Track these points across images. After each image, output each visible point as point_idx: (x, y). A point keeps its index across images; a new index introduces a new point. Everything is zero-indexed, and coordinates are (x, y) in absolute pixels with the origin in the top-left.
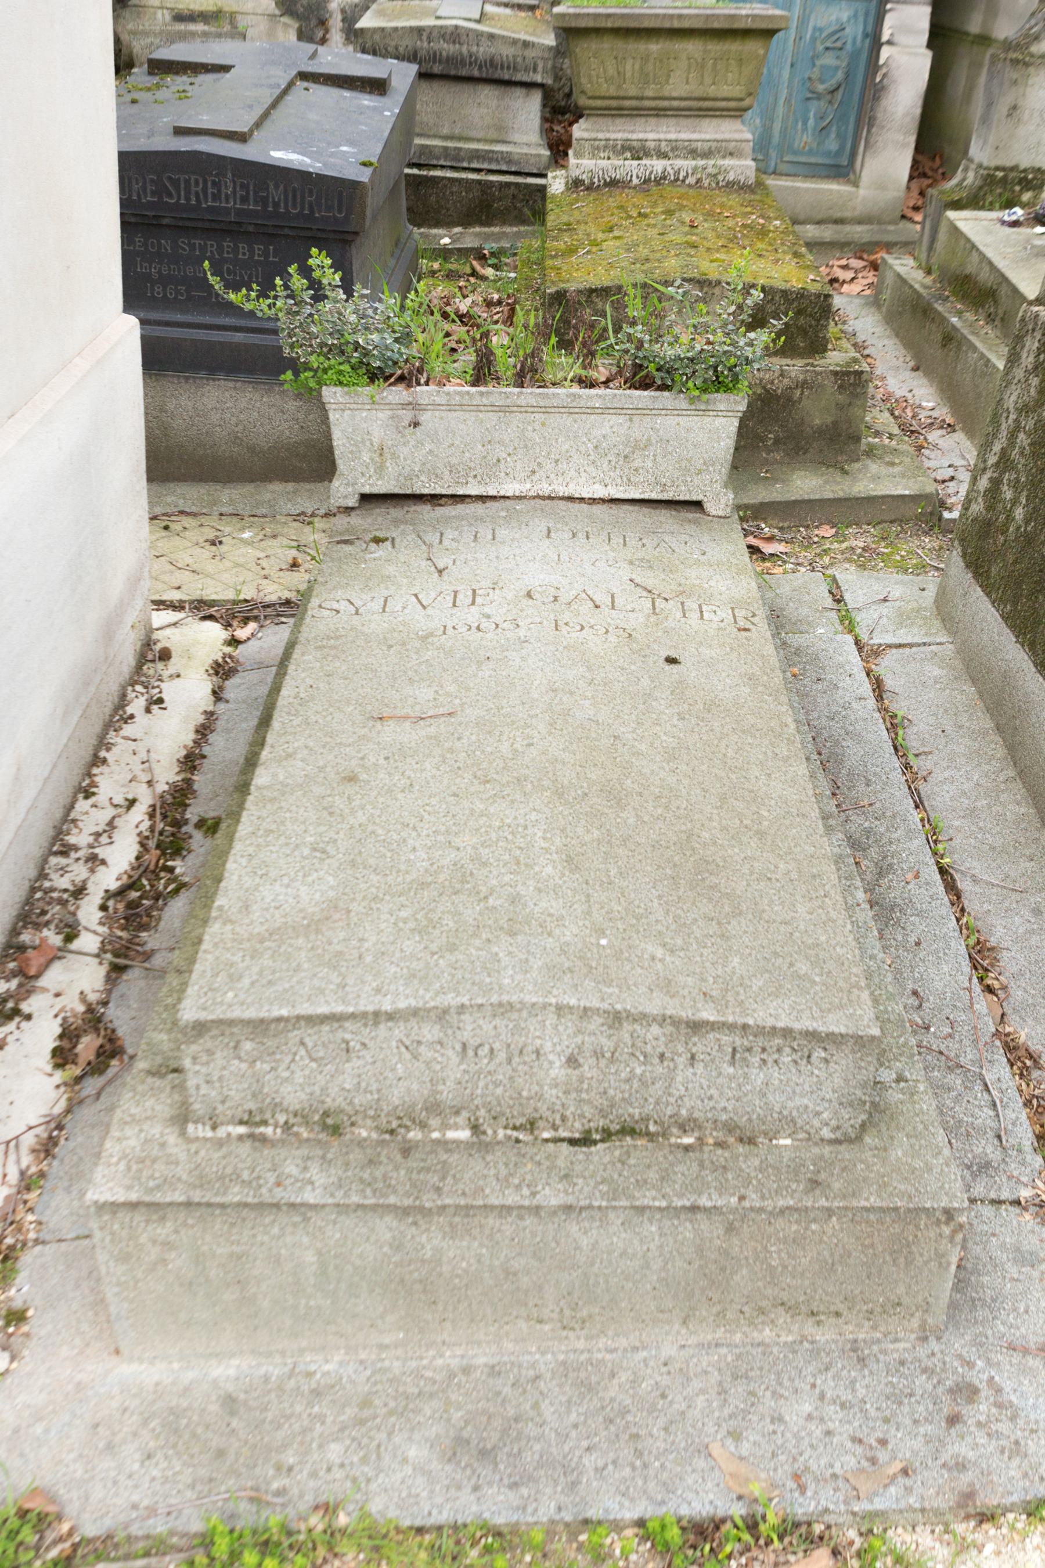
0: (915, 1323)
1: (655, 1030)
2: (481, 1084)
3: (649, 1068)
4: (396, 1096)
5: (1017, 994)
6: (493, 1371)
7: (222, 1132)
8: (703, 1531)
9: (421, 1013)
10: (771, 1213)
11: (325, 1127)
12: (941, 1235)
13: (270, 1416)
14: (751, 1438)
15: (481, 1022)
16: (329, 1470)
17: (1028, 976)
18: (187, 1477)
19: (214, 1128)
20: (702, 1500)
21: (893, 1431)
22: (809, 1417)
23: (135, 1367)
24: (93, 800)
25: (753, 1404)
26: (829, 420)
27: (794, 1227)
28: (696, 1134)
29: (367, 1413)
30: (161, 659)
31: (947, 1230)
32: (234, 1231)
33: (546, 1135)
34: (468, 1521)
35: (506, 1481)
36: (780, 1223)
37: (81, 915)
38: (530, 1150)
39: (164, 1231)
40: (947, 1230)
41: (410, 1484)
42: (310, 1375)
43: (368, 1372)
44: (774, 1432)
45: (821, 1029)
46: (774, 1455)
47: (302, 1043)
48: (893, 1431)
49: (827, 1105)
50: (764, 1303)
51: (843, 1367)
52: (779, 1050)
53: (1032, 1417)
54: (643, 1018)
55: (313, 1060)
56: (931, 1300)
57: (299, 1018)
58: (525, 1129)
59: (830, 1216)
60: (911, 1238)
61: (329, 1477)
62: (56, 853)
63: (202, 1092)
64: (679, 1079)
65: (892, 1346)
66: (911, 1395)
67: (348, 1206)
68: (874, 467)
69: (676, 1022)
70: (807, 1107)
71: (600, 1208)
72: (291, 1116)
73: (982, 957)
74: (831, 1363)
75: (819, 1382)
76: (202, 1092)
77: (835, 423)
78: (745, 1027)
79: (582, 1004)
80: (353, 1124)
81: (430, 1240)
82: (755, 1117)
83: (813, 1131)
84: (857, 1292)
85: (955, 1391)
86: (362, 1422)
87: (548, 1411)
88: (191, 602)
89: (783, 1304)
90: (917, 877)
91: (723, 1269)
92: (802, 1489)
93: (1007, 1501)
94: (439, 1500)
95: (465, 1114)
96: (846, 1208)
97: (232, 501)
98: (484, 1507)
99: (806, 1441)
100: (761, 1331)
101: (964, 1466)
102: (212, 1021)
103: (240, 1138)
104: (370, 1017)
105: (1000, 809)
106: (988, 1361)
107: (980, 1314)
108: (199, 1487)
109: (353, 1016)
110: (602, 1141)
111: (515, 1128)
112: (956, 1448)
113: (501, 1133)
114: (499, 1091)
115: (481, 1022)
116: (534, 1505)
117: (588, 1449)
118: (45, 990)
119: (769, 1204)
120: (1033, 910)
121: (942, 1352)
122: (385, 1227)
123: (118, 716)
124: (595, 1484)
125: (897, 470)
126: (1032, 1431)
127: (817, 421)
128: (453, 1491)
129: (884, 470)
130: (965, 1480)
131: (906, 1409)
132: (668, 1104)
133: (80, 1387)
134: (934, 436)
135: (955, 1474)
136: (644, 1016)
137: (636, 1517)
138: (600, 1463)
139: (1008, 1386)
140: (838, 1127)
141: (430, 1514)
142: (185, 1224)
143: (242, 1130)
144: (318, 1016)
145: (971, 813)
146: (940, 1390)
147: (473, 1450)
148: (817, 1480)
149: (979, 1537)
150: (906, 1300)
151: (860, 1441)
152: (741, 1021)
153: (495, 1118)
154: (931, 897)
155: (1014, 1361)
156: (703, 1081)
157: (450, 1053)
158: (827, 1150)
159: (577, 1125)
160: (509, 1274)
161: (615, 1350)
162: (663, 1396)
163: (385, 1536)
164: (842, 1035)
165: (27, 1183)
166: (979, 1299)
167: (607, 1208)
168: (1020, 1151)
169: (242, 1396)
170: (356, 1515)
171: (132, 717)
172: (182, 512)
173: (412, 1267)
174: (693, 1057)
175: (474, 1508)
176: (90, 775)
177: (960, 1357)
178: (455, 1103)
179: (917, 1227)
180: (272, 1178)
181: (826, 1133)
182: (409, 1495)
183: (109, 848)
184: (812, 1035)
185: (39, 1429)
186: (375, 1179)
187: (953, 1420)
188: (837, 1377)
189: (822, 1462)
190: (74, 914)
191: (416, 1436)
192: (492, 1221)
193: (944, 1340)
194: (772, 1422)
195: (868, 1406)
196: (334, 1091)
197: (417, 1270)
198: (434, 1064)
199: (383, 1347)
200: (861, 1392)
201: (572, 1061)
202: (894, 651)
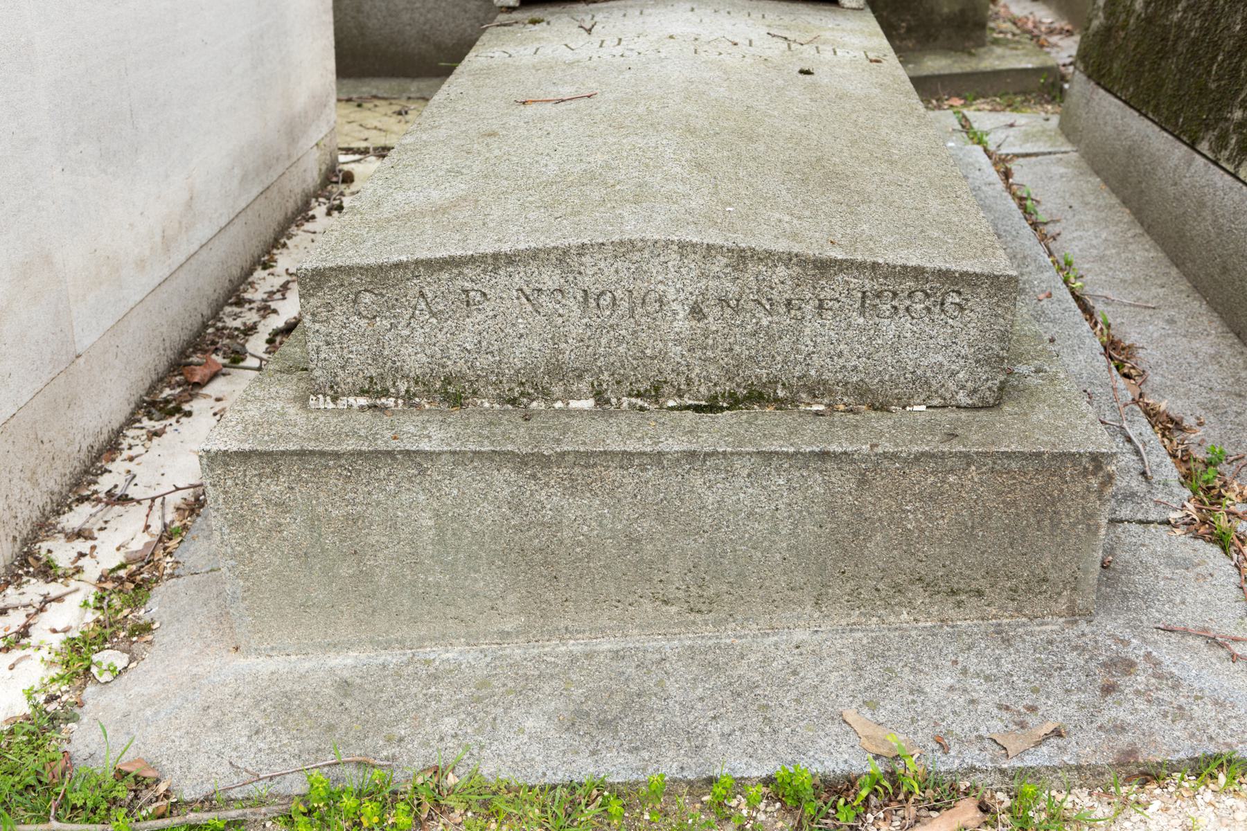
0: (1063, 605)
1: (782, 271)
2: (604, 341)
3: (776, 318)
4: (517, 357)
5: (1154, 379)
6: (617, 655)
7: (342, 403)
8: (837, 788)
9: (541, 255)
10: (905, 460)
11: (446, 397)
12: (1088, 488)
13: (385, 696)
14: (889, 707)
15: (602, 264)
16: (442, 739)
17: (1165, 366)
18: (295, 747)
19: (334, 399)
20: (835, 758)
21: (1043, 699)
22: (951, 688)
23: (252, 659)
24: (271, 270)
25: (890, 679)
26: (957, 8)
27: (931, 479)
28: (826, 401)
29: (484, 692)
30: (344, 182)
31: (1094, 483)
32: (350, 487)
33: (671, 403)
34: (585, 781)
35: (626, 746)
36: (915, 473)
37: (248, 346)
38: (655, 416)
39: (276, 488)
40: (1094, 483)
41: (528, 749)
42: (428, 662)
43: (488, 659)
44: (914, 702)
45: (954, 268)
46: (913, 721)
47: (422, 295)
48: (1043, 699)
49: (962, 362)
50: (900, 579)
51: (987, 647)
52: (910, 296)
53: (1196, 685)
54: (769, 257)
55: (433, 315)
56: (1080, 574)
57: (417, 263)
58: (650, 397)
59: (969, 465)
60: (1056, 493)
61: (442, 745)
62: (231, 304)
63: (323, 356)
64: (807, 331)
65: (1038, 629)
66: (1061, 669)
67: (465, 453)
68: (999, 51)
69: (802, 261)
70: (941, 365)
71: (724, 453)
72: (412, 383)
73: (1116, 351)
74: (973, 644)
75: (960, 659)
76: (323, 356)
77: (962, 12)
78: (875, 266)
79: (705, 242)
80: (475, 393)
81: (550, 497)
82: (887, 378)
83: (948, 396)
84: (999, 564)
85: (1109, 665)
86: (479, 700)
87: (672, 687)
88: (375, 149)
89: (920, 579)
90: (1050, 296)
91: (856, 534)
92: (945, 749)
93: (1175, 758)
94: (555, 763)
95: (588, 378)
96: (985, 454)
97: (419, 90)
98: (602, 769)
99: (949, 709)
100: (898, 614)
101: (1123, 729)
102: (331, 269)
103: (362, 408)
104: (490, 261)
105: (1130, 255)
106: (1144, 640)
107: (1133, 603)
108: (305, 756)
109: (472, 260)
110: (728, 409)
111: (639, 395)
112: (1113, 713)
113: (625, 401)
114: (622, 349)
115: (602, 264)
116: (656, 766)
117: (714, 718)
118: (206, 396)
119: (904, 450)
120: (1167, 321)
121: (1093, 633)
122: (503, 480)
123: (302, 214)
124: (720, 747)
125: (1019, 52)
126: (1197, 698)
127: (946, 10)
128: (569, 756)
129: (1008, 52)
130: (1124, 741)
131: (1056, 681)
132: (796, 362)
133: (195, 677)
134: (1054, 39)
135: (1115, 736)
136: (770, 254)
137: (764, 775)
138: (727, 730)
139: (1167, 660)
140: (975, 391)
141: (544, 774)
142: (299, 479)
143: (363, 401)
144: (437, 261)
145: (1101, 258)
146: (1092, 664)
147: (591, 722)
148: (960, 741)
149: (1143, 798)
150: (1053, 575)
151: (1007, 708)
152: (870, 259)
153: (618, 383)
154: (1064, 310)
155: (1172, 640)
156: (832, 333)
157: (571, 303)
158: (964, 415)
159: (703, 389)
160: (634, 540)
161: (745, 636)
162: (795, 673)
163: (494, 793)
164: (976, 275)
165: (168, 533)
166: (1131, 593)
167: (732, 454)
168: (1165, 484)
169: (358, 681)
170: (465, 778)
171: (313, 217)
172: (375, 97)
173: (531, 533)
174: (821, 307)
175: (591, 770)
176: (269, 253)
177: (1113, 636)
178: (578, 364)
179: (1062, 477)
180: (388, 434)
181: (962, 398)
182: (523, 760)
183: (281, 303)
184: (944, 275)
185: (148, 713)
186: (494, 435)
187: (1108, 689)
188: (980, 654)
189: (966, 726)
190: (243, 345)
191: (534, 710)
192: (614, 474)
193: (1095, 622)
194: (911, 693)
195: (1015, 678)
196: (454, 352)
197: (537, 536)
198: (555, 317)
199: (505, 635)
200: (1007, 667)
201: (696, 312)
202: (1021, 160)
